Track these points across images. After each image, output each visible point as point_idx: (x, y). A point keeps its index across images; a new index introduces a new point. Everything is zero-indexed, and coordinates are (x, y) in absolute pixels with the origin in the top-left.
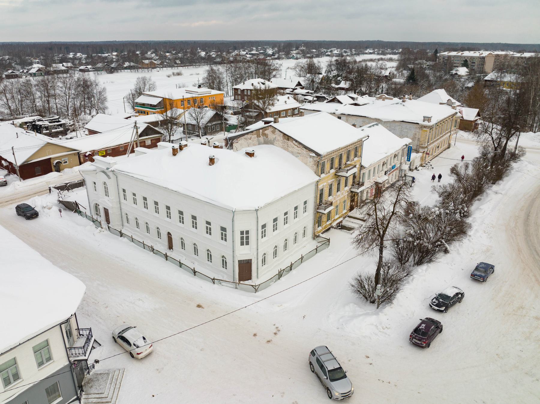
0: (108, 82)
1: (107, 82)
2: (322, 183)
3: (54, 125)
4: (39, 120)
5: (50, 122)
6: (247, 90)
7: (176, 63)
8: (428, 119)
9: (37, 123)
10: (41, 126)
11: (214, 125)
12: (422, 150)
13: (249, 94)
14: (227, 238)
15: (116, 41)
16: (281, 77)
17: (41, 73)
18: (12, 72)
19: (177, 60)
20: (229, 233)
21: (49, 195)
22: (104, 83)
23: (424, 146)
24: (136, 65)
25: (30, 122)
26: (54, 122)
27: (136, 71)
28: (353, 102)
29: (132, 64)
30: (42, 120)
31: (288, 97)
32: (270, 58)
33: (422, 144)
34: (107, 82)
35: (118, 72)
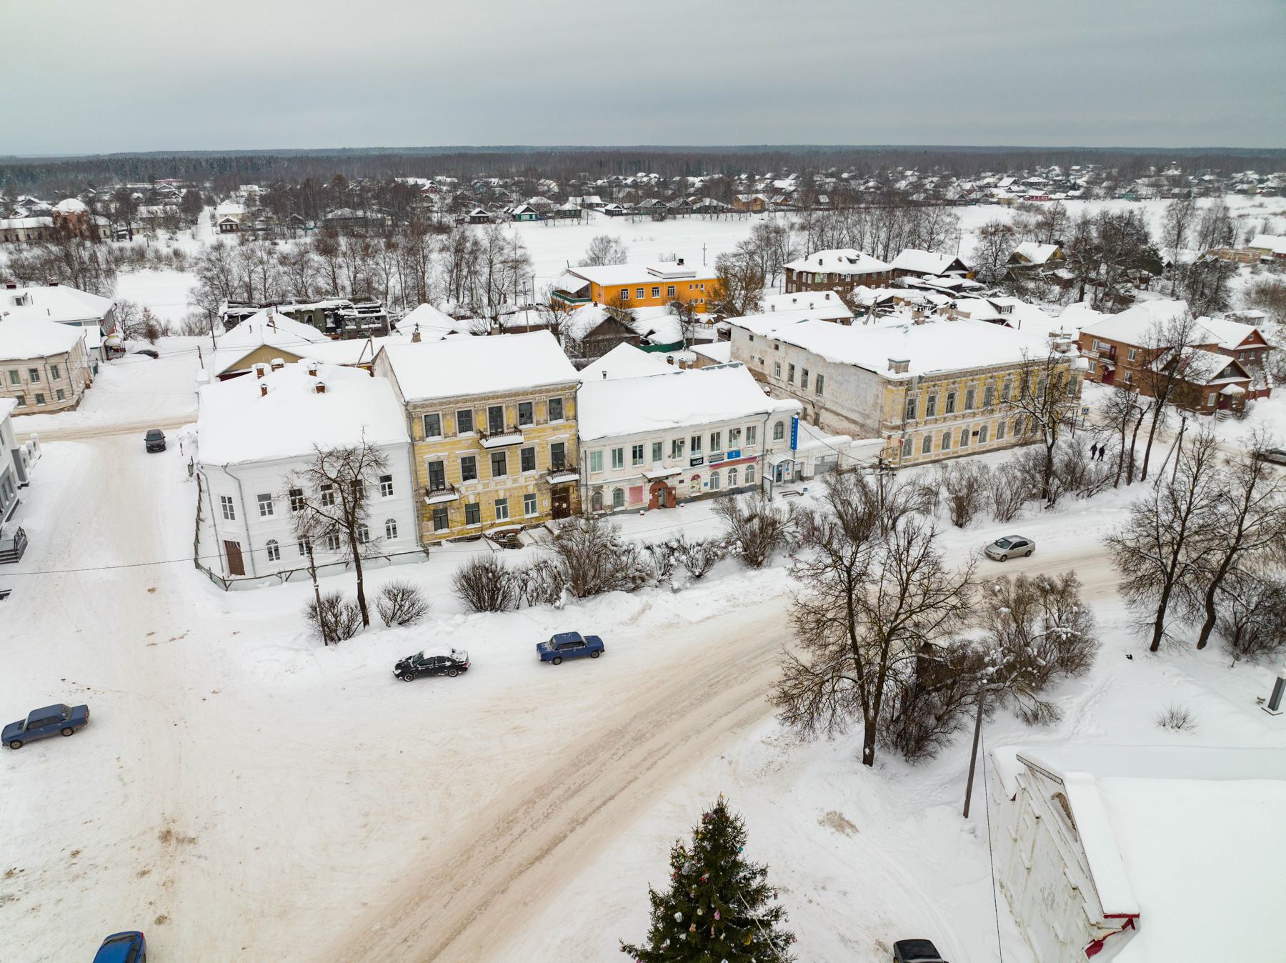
0: (644, 238)
1: (642, 239)
2: (437, 451)
3: (372, 318)
4: (346, 307)
5: (360, 312)
6: (808, 273)
7: (818, 202)
8: (900, 366)
9: (341, 312)
10: (343, 316)
11: (607, 340)
12: (886, 433)
13: (810, 282)
14: (235, 513)
15: (766, 146)
16: (525, 254)
17: (531, 216)
18: (481, 212)
19: (1182, 172)
20: (236, 504)
21: (1044, 514)
22: (635, 241)
23: (889, 424)
24: (720, 204)
25: (330, 310)
26: (373, 312)
27: (729, 219)
28: (997, 316)
29: (715, 203)
30: (351, 308)
31: (828, 295)
32: (1063, 195)
33: (886, 420)
34: (642, 239)
35: (675, 218)
